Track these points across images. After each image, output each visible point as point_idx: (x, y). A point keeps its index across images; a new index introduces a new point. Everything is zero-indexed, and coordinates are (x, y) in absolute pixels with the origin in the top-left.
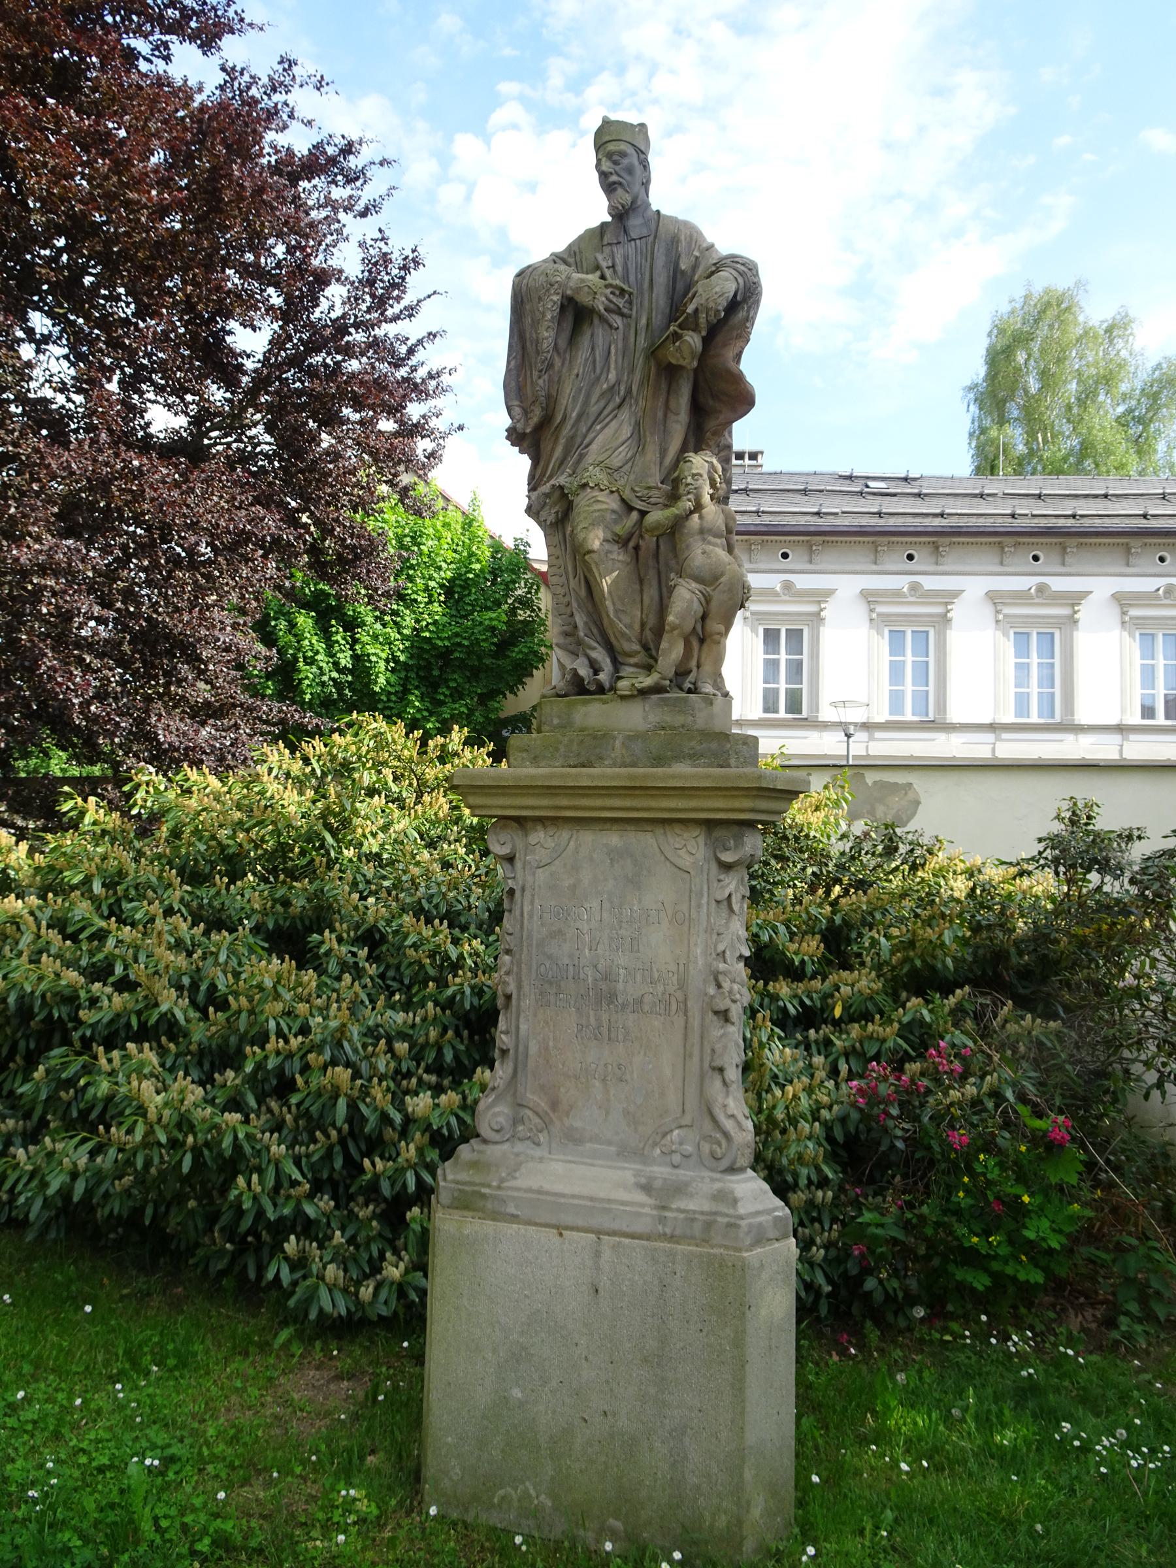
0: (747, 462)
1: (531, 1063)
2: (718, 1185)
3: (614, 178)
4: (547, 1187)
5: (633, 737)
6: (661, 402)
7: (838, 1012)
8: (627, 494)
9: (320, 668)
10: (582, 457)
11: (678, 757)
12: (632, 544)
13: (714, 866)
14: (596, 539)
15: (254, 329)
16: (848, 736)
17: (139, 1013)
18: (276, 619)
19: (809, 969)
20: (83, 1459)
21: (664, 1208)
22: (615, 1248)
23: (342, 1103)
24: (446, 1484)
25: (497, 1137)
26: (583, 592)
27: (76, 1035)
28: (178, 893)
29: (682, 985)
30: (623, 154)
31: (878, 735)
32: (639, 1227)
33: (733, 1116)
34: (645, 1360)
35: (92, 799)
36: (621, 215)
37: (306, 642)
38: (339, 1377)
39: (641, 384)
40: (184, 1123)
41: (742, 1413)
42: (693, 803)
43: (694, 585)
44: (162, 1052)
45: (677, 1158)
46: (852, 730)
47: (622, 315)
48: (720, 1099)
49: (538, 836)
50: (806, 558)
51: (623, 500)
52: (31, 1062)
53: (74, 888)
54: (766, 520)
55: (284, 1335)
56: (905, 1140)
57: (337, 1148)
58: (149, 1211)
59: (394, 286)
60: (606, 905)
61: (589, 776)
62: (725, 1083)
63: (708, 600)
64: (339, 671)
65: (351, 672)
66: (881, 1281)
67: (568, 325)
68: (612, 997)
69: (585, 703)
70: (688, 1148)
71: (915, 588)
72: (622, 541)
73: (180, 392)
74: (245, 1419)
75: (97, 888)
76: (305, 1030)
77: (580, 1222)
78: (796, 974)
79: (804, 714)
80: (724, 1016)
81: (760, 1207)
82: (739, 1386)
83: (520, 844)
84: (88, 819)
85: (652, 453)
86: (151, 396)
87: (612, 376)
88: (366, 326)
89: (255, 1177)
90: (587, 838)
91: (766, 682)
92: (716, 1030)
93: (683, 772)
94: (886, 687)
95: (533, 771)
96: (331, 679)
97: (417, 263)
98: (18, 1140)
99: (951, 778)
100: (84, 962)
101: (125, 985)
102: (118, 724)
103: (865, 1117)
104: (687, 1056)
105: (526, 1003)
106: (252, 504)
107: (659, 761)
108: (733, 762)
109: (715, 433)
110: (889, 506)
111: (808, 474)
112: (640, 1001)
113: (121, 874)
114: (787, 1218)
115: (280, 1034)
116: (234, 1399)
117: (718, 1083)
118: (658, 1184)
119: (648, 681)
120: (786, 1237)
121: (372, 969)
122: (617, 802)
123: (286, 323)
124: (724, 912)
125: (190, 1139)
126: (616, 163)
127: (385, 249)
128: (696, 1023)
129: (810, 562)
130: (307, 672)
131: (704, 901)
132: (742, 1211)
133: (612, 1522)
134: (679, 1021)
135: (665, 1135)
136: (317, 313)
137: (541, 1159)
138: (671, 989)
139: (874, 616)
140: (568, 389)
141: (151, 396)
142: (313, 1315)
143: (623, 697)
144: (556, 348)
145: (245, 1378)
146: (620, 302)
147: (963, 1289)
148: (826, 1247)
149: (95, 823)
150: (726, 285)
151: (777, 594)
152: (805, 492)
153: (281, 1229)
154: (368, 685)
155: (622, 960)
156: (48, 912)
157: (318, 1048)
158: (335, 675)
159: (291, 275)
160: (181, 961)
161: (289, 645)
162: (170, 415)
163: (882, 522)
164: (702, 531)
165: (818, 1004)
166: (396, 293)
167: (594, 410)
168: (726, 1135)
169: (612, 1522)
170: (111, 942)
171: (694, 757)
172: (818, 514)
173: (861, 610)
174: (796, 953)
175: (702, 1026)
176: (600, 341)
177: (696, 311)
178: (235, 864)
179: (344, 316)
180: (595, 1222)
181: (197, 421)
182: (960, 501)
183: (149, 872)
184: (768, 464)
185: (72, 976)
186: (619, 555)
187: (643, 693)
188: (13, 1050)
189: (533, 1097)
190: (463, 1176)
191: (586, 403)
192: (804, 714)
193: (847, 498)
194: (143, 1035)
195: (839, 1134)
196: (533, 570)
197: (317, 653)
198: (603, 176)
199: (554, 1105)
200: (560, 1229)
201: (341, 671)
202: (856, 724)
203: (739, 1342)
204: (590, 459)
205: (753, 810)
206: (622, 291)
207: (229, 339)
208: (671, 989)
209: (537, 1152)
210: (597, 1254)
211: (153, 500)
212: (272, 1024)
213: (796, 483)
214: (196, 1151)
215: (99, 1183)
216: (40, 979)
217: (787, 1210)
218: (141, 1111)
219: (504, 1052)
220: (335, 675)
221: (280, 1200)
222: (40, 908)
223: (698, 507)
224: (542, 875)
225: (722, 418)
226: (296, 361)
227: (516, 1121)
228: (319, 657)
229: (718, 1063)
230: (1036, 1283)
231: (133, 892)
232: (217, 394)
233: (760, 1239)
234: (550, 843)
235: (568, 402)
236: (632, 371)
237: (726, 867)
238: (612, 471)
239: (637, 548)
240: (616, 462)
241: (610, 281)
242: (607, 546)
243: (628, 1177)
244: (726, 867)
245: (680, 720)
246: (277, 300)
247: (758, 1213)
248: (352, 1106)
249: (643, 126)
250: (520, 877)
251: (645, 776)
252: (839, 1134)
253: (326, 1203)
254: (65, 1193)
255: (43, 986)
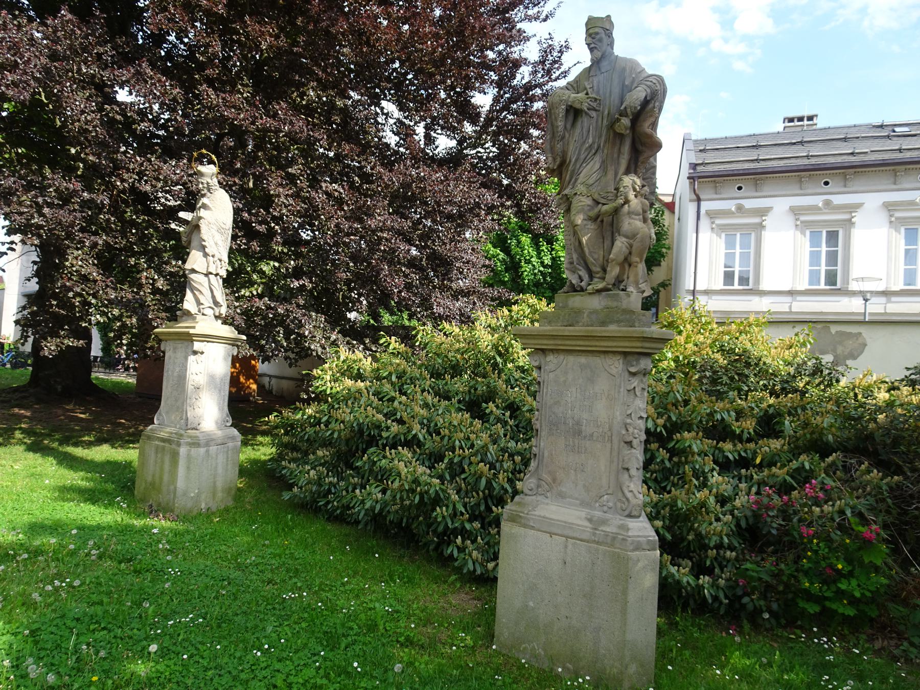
0: (806, 122)
1: (545, 460)
2: (621, 522)
3: (592, 46)
4: (547, 515)
5: (594, 312)
6: (616, 150)
7: (758, 461)
8: (596, 196)
9: (534, 266)
10: (576, 180)
11: (611, 322)
12: (599, 219)
13: (627, 373)
14: (579, 220)
15: (485, 93)
16: (866, 300)
17: (405, 434)
18: (511, 239)
19: (746, 436)
20: (365, 605)
21: (596, 529)
22: (573, 544)
23: (484, 481)
24: (502, 639)
25: (530, 493)
26: (577, 244)
27: (380, 442)
28: (428, 383)
29: (610, 430)
30: (597, 33)
31: (894, 299)
32: (584, 537)
33: (631, 491)
34: (584, 596)
35: (393, 338)
36: (596, 63)
37: (526, 252)
38: (474, 599)
39: (605, 142)
40: (416, 481)
41: (625, 624)
42: (615, 344)
43: (624, 239)
44: (415, 452)
45: (605, 508)
46: (868, 296)
47: (596, 110)
48: (627, 483)
49: (551, 358)
50: (842, 184)
51: (594, 200)
52: (364, 452)
53: (384, 378)
54: (813, 161)
55: (453, 577)
56: (778, 529)
57: (483, 501)
58: (405, 520)
59: (555, 62)
60: (579, 390)
61: (569, 331)
62: (630, 476)
63: (631, 246)
64: (544, 267)
65: (551, 267)
66: (752, 600)
67: (571, 118)
68: (580, 433)
69: (573, 296)
70: (611, 504)
71: (740, 208)
72: (594, 219)
73: (453, 129)
74: (431, 606)
75: (394, 378)
76: (472, 446)
77: (559, 532)
78: (737, 438)
79: (838, 286)
80: (629, 444)
81: (641, 534)
82: (624, 611)
83: (543, 362)
84: (391, 347)
85: (610, 175)
86: (439, 131)
87: (590, 141)
88: (540, 86)
89: (444, 508)
90: (571, 359)
91: (811, 265)
92: (626, 451)
93: (612, 329)
94: (902, 267)
95: (549, 328)
96: (540, 271)
97: (567, 47)
98: (359, 487)
99: (889, 329)
100: (385, 411)
101: (401, 422)
102: (414, 301)
103: (756, 515)
104: (612, 462)
105: (543, 434)
106: (479, 188)
107: (603, 323)
108: (637, 324)
109: (643, 163)
110: (907, 144)
111: (849, 127)
112: (592, 435)
113: (404, 372)
114: (654, 541)
115: (461, 447)
116: (428, 598)
117: (626, 476)
118: (595, 519)
119: (601, 286)
120: (655, 550)
121: (511, 422)
122: (581, 343)
123: (500, 89)
124: (632, 396)
125: (419, 489)
126: (593, 38)
127: (550, 43)
128: (616, 447)
129: (845, 186)
130: (526, 268)
131: (622, 390)
132: (630, 534)
133: (568, 665)
134: (609, 445)
135: (601, 497)
136: (515, 82)
137: (547, 504)
138: (606, 430)
139: (893, 219)
140: (571, 148)
141: (439, 131)
142: (465, 571)
143: (590, 294)
144: (565, 127)
145: (434, 591)
146: (594, 105)
147: (803, 613)
148: (727, 580)
149: (394, 349)
150: (639, 94)
151: (820, 209)
152: (845, 139)
153: (455, 532)
154: (559, 274)
155: (585, 416)
156: (374, 388)
157: (475, 455)
158: (542, 269)
159: (501, 65)
160: (424, 412)
161: (517, 254)
162: (448, 140)
163: (900, 155)
164: (629, 213)
165: (750, 456)
166: (557, 66)
167: (582, 157)
168: (628, 499)
169: (568, 665)
170: (396, 403)
171: (618, 322)
172: (852, 154)
173: (883, 217)
174: (738, 427)
175: (619, 448)
176: (586, 124)
177: (625, 108)
178: (456, 370)
179: (529, 82)
180: (566, 532)
181: (460, 143)
182: (780, 149)
183: (416, 373)
184: (820, 123)
185: (380, 416)
186: (591, 226)
187: (599, 291)
188: (357, 449)
189: (545, 476)
190: (513, 508)
191: (579, 154)
192: (838, 286)
193: (877, 140)
194: (408, 444)
195: (743, 524)
196: (661, 201)
197: (532, 257)
198: (588, 45)
199: (554, 480)
200: (551, 534)
201: (545, 266)
202: (871, 292)
203: (625, 592)
204: (579, 181)
205: (642, 348)
206: (596, 100)
207: (473, 100)
208: (606, 430)
209: (546, 501)
210: (566, 547)
211: (430, 191)
212: (457, 443)
213: (839, 134)
214: (421, 495)
215: (385, 507)
216: (367, 417)
217: (657, 538)
218: (399, 474)
219: (535, 455)
220: (542, 269)
221: (455, 520)
222: (370, 387)
223: (627, 201)
224: (552, 375)
225: (645, 155)
226: (506, 108)
227: (538, 486)
228: (533, 259)
229: (626, 466)
230: (849, 616)
231: (409, 381)
232: (468, 128)
233: (638, 547)
234: (555, 361)
235: (572, 155)
236: (600, 137)
237: (633, 374)
238: (589, 186)
239: (602, 221)
240: (591, 181)
241: (590, 95)
242: (585, 222)
243: (583, 515)
244: (633, 374)
245: (615, 304)
246: (494, 77)
247: (639, 536)
248: (489, 482)
249: (609, 17)
250: (544, 377)
251: (592, 331)
252: (743, 524)
253: (477, 525)
254: (372, 508)
255: (368, 420)
